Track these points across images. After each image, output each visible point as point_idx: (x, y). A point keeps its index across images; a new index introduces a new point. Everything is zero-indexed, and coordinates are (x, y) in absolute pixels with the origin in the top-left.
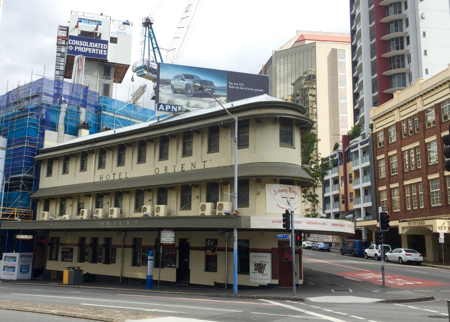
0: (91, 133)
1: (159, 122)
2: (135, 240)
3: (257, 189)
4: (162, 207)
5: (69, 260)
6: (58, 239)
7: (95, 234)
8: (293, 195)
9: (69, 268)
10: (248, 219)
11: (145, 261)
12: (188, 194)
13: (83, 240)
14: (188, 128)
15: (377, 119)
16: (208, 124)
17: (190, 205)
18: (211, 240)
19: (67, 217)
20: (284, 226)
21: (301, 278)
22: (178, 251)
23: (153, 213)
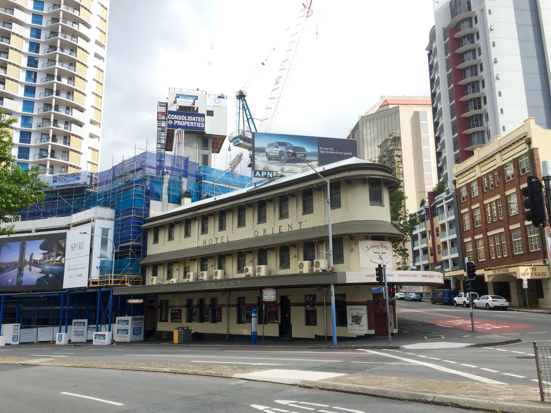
0: (193, 201)
1: (256, 187)
2: (239, 299)
3: (350, 245)
4: (263, 267)
5: (178, 320)
6: (167, 301)
7: (201, 296)
8: (384, 250)
9: (178, 329)
12: (286, 254)
13: (190, 301)
14: (284, 192)
17: (289, 264)
18: (310, 296)
19: (174, 280)
20: (377, 279)
21: (395, 328)
23: (255, 274)
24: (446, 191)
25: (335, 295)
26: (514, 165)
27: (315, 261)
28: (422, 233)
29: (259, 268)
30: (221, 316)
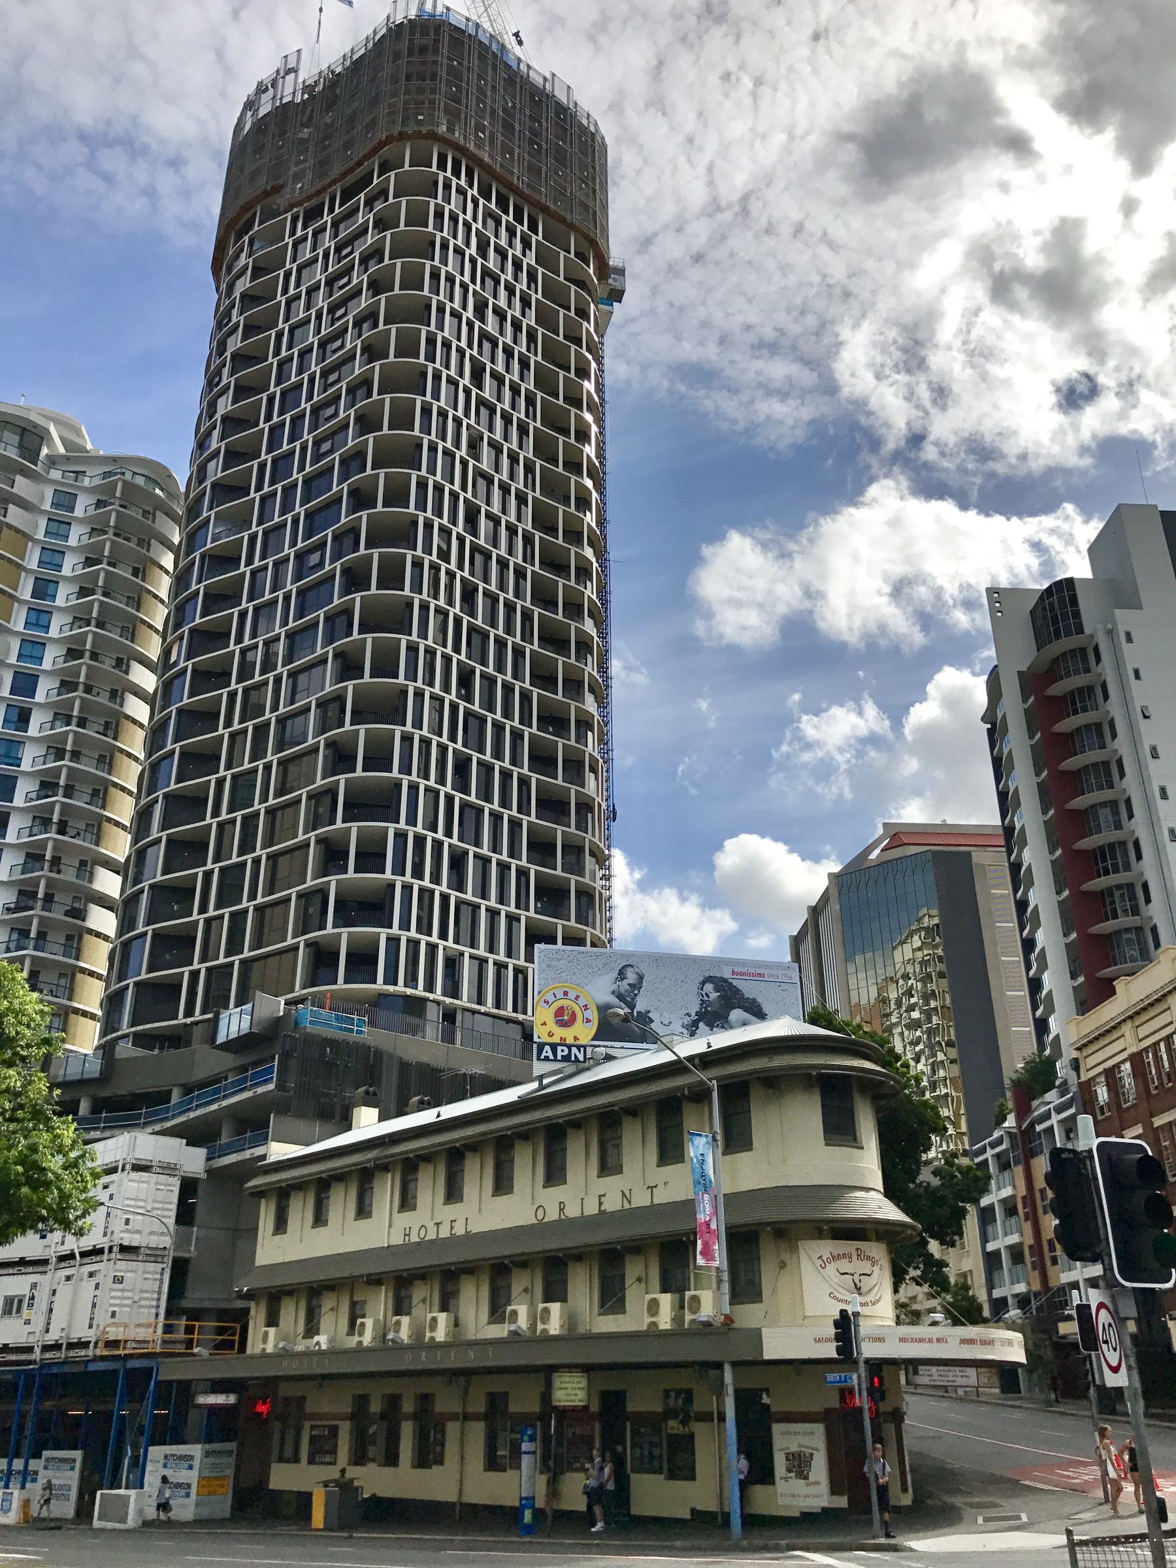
0: (382, 1118)
1: (542, 1087)
3: (779, 1254)
4: (555, 1308)
5: (328, 1459)
6: (301, 1401)
7: (393, 1387)
8: (866, 1267)
9: (326, 1484)
10: (756, 1336)
11: (516, 1454)
12: (616, 1272)
13: (362, 1401)
14: (611, 1105)
15: (1085, 1045)
16: (657, 1093)
17: (622, 1301)
18: (678, 1392)
19: (322, 1340)
20: (839, 1350)
21: (904, 1490)
22: (597, 1426)
23: (533, 1327)
24: (1059, 1087)
25: (736, 1391)
26: (1107, 1078)
27: (688, 1294)
28: (1003, 1201)
29: (546, 1311)
30: (443, 1445)
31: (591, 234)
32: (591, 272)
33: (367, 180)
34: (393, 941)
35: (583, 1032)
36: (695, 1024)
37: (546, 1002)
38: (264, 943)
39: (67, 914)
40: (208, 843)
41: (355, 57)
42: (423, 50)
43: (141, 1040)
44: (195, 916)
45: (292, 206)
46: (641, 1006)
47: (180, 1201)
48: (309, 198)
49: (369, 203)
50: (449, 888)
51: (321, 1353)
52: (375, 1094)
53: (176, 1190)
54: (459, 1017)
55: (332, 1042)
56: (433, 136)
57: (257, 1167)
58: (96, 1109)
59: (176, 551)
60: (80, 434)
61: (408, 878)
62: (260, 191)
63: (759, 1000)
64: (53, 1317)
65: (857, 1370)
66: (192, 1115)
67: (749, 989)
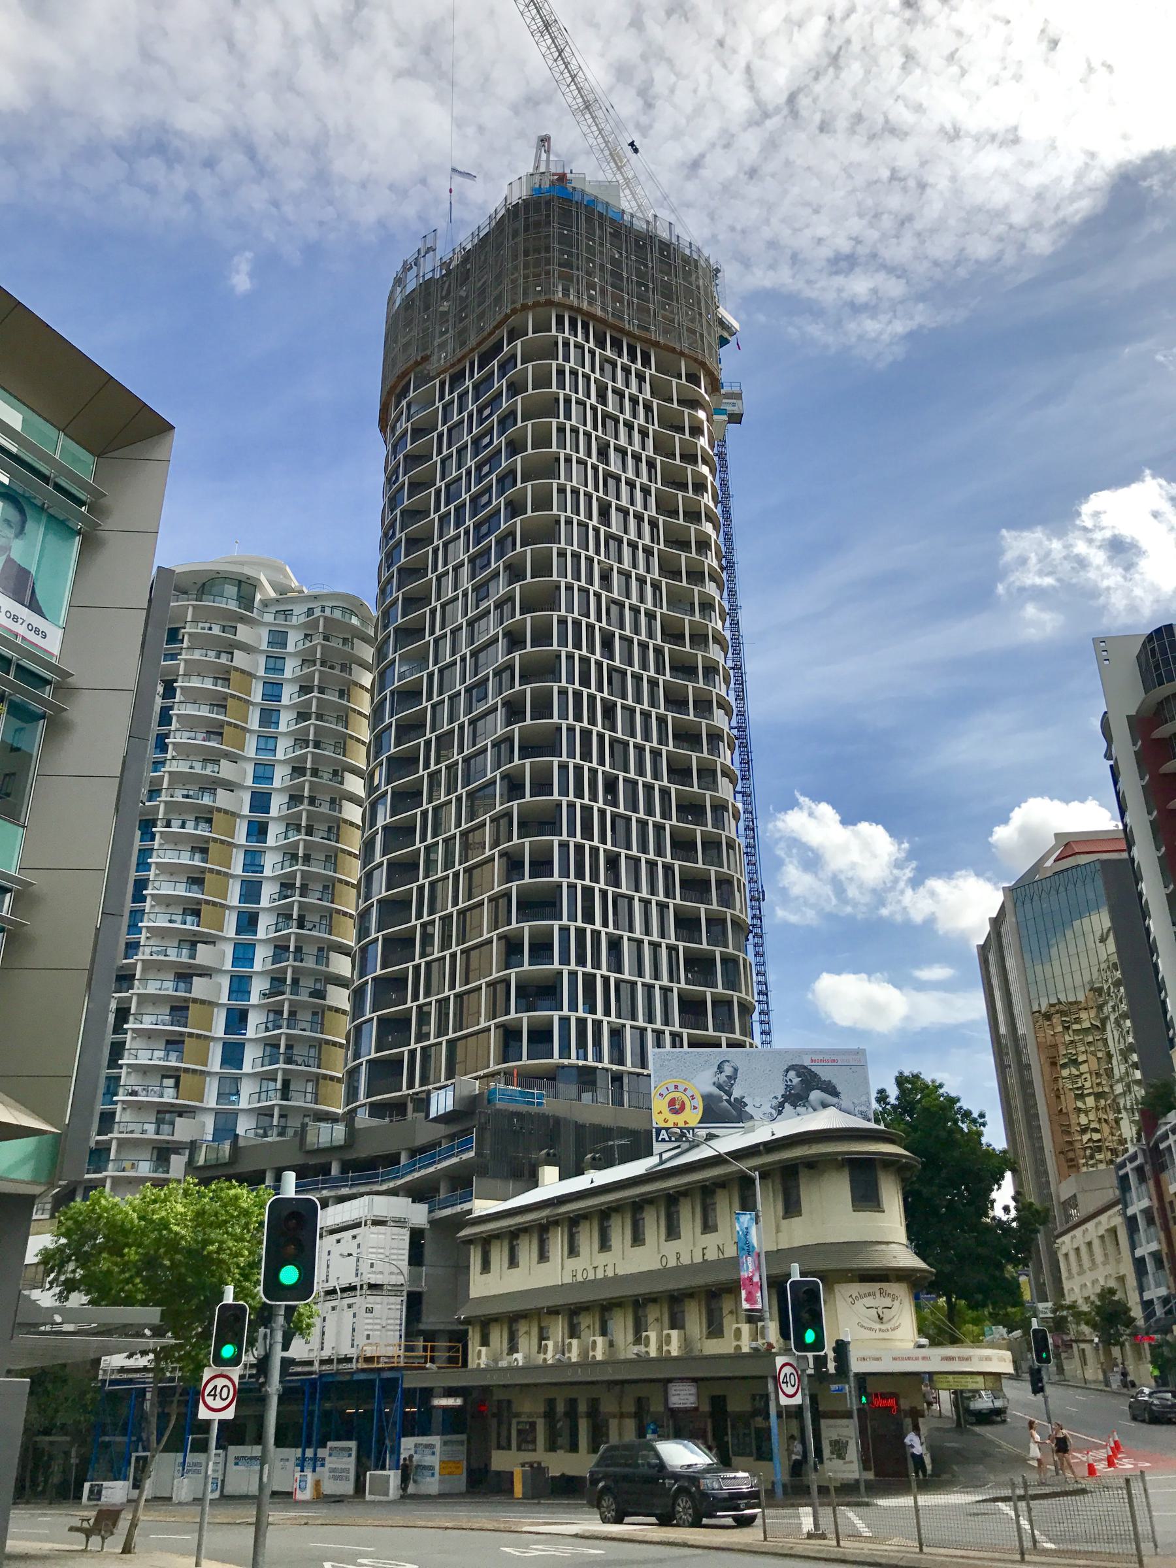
0: (562, 1177)
1: (662, 1162)
2: (639, 1401)
5: (530, 1447)
8: (887, 1302)
9: (523, 1465)
13: (551, 1403)
19: (519, 1356)
31: (700, 357)
32: (703, 391)
33: (498, 347)
34: (565, 1021)
35: (692, 1117)
36: (781, 1105)
37: (661, 1095)
38: (464, 1025)
39: (312, 995)
40: (415, 939)
41: (482, 235)
42: (537, 225)
43: (377, 1110)
44: (409, 1004)
45: (439, 375)
46: (736, 1093)
47: (411, 1243)
48: (452, 366)
49: (503, 368)
50: (609, 971)
51: (518, 1368)
52: (554, 1155)
53: (407, 1238)
54: (625, 1080)
55: (519, 1115)
56: (550, 303)
57: (462, 1221)
58: (344, 1170)
59: (371, 691)
60: (286, 576)
61: (573, 966)
62: (412, 362)
63: (834, 1081)
64: (326, 1336)
65: (848, 1382)
66: (416, 1175)
67: (825, 1074)
